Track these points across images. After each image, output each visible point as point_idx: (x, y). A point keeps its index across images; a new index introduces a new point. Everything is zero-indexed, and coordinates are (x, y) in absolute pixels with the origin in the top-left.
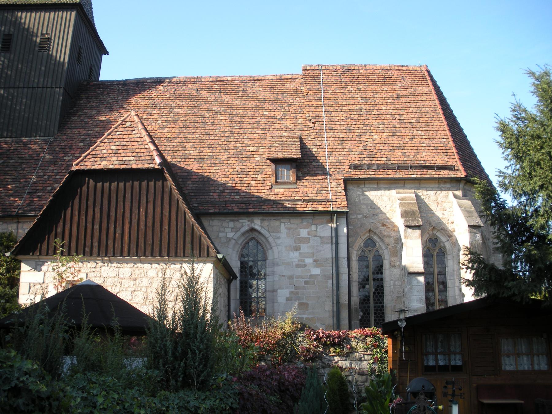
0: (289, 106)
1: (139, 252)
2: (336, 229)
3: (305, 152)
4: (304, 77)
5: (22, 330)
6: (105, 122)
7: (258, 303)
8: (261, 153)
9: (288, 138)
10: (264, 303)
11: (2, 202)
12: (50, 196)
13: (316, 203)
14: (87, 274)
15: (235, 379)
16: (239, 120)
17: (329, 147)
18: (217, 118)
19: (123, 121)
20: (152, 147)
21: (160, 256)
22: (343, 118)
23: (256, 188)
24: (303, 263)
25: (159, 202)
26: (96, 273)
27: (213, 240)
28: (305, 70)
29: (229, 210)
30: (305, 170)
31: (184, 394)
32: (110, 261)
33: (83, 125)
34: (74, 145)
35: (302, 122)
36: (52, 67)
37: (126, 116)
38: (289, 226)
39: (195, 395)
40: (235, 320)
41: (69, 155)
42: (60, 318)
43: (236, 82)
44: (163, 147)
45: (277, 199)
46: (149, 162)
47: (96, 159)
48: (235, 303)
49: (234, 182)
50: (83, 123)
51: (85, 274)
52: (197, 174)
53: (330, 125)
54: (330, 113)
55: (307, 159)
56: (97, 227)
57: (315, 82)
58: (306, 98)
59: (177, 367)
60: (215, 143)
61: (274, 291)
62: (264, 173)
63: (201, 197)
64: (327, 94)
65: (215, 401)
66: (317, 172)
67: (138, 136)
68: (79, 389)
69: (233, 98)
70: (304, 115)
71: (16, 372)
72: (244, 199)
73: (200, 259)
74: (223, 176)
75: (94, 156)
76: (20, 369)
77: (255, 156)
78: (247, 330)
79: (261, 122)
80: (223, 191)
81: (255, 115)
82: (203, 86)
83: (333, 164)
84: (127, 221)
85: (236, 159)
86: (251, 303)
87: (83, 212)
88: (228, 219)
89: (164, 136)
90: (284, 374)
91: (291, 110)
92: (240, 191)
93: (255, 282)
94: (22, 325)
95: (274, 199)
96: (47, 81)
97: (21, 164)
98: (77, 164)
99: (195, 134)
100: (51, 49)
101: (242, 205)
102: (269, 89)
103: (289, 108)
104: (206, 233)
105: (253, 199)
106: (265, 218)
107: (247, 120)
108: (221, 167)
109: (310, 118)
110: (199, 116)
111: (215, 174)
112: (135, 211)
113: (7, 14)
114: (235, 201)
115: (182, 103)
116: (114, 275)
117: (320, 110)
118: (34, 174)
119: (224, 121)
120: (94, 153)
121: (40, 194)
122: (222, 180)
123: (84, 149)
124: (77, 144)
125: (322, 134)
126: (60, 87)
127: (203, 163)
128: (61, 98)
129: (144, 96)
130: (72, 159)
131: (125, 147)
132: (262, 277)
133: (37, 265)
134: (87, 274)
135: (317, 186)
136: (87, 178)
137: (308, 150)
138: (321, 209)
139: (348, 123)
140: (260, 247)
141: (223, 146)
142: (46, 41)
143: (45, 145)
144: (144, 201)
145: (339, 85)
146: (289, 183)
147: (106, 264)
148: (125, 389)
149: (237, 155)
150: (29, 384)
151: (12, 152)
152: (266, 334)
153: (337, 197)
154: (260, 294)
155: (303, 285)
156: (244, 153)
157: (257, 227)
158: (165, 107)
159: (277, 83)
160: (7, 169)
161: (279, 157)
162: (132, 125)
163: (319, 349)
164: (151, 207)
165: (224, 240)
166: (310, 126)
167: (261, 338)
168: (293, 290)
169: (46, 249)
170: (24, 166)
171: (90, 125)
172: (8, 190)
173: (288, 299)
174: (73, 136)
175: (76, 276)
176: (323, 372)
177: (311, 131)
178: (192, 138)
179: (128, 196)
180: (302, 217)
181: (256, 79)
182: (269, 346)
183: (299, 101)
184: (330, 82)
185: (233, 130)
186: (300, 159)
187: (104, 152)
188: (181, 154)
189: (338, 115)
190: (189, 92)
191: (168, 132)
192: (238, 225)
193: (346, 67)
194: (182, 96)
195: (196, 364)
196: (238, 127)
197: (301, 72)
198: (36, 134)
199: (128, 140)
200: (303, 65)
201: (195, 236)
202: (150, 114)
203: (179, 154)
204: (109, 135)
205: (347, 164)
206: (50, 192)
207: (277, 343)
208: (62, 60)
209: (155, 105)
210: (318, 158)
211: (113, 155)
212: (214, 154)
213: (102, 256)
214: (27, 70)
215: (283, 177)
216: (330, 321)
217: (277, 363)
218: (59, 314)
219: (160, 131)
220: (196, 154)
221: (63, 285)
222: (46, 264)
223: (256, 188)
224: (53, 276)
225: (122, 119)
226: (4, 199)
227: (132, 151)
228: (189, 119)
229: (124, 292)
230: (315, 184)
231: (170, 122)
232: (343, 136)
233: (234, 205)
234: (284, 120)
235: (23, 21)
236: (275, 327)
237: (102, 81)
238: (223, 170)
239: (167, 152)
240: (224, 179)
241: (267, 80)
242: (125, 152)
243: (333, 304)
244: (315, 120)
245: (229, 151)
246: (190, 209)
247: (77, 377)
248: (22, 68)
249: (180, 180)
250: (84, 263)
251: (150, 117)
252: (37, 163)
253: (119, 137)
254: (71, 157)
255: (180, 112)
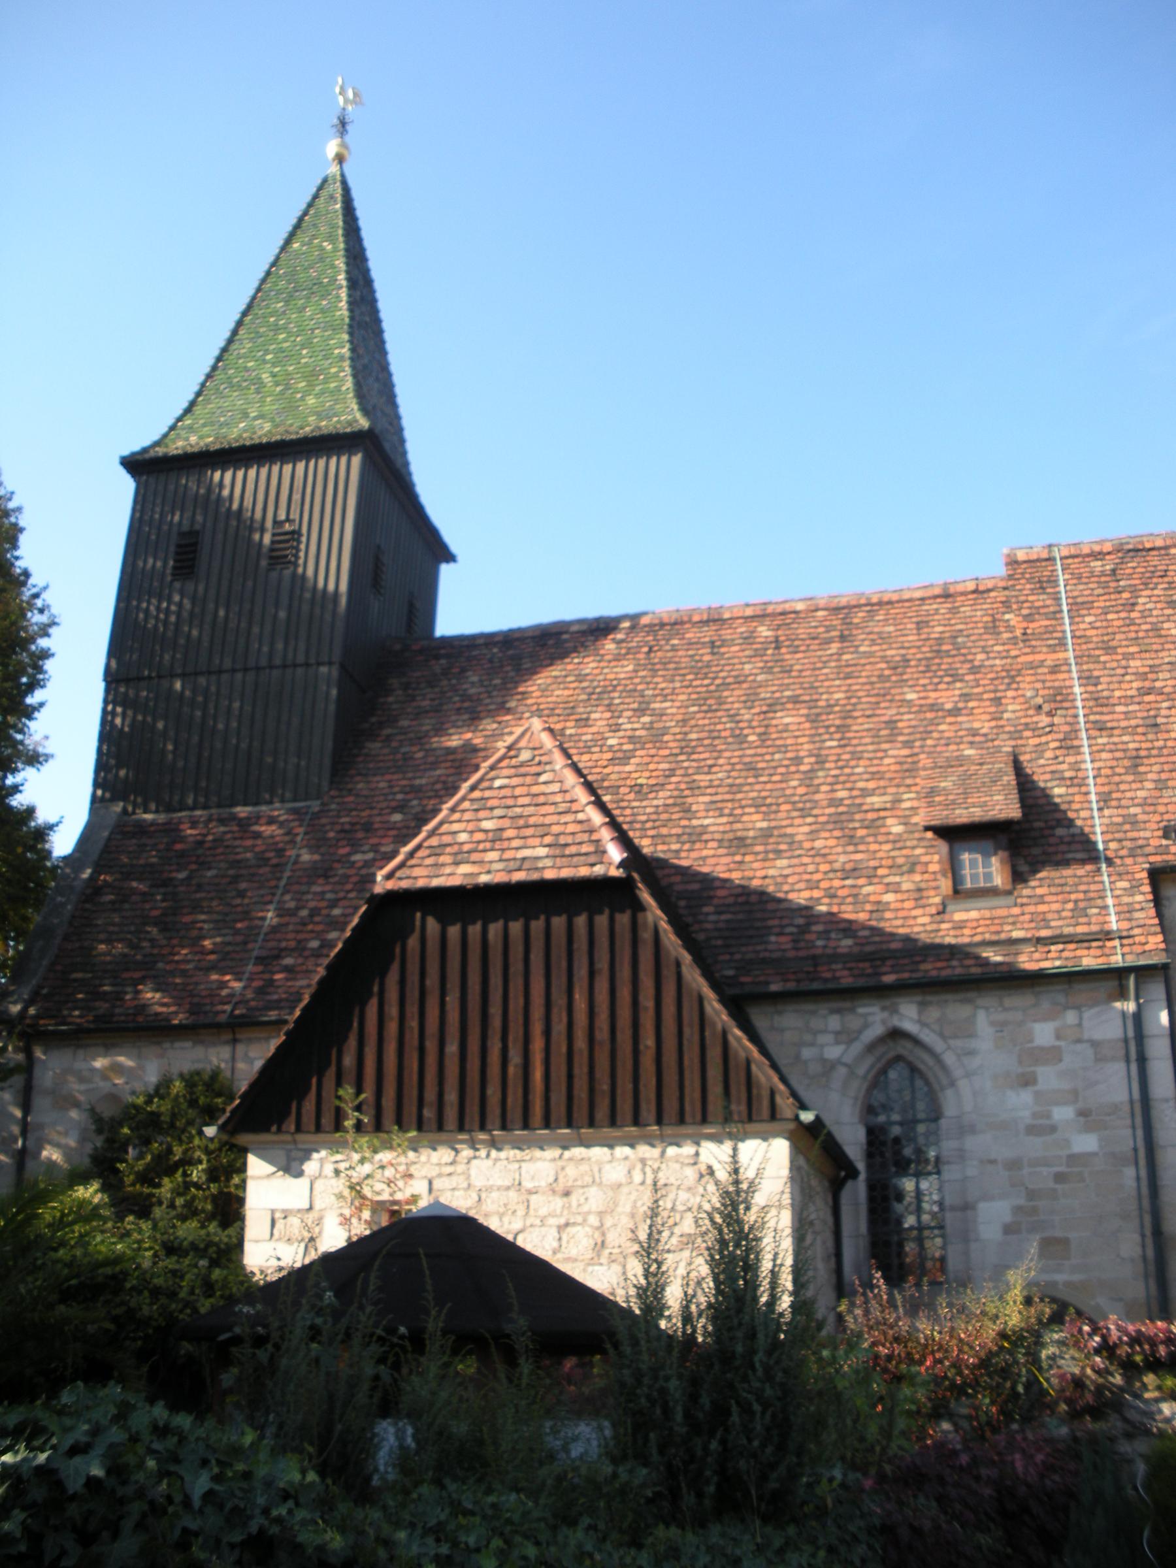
0: (975, 670)
1: (575, 1115)
2: (1138, 1017)
3: (1030, 802)
4: (1011, 583)
5: (263, 1355)
6: (460, 751)
7: (920, 1241)
8: (907, 813)
9: (981, 764)
10: (938, 1241)
11: (191, 987)
12: (317, 965)
13: (1072, 946)
14: (430, 1183)
15: (868, 1483)
16: (838, 722)
17: (1099, 780)
18: (774, 722)
19: (510, 748)
20: (597, 818)
21: (636, 1122)
22: (1133, 692)
23: (901, 914)
24: (1047, 1122)
25: (624, 973)
26: (454, 1178)
27: (785, 1070)
28: (1012, 562)
29: (826, 980)
30: (1036, 851)
31: (723, 1535)
32: (494, 1144)
33: (400, 763)
34: (378, 819)
35: (1018, 714)
36: (306, 608)
37: (518, 731)
38: (1001, 1017)
39: (754, 1536)
40: (859, 1300)
41: (366, 848)
42: (363, 1318)
43: (820, 613)
44: (628, 812)
45: (961, 940)
46: (592, 859)
47: (442, 859)
48: (854, 1248)
49: (835, 901)
50: (399, 756)
51: (425, 1184)
52: (728, 885)
53: (1098, 717)
54: (1093, 681)
55: (1039, 820)
56: (452, 1048)
57: (1045, 597)
58: (1021, 645)
59: (699, 1453)
60: (775, 794)
61: (967, 1207)
62: (919, 868)
63: (743, 949)
64: (1082, 626)
65: (814, 1555)
66: (1070, 856)
67: (555, 787)
68: (427, 1531)
69: (816, 660)
70: (1020, 692)
71: (259, 1492)
72: (868, 949)
73: (750, 1127)
74: (802, 885)
75: (436, 851)
76: (269, 1483)
77: (889, 821)
78: (896, 1328)
79: (900, 725)
80: (804, 929)
81: (882, 705)
82: (727, 634)
83: (1115, 828)
84: (537, 1029)
85: (837, 833)
86: (900, 1245)
87: (412, 1010)
88: (823, 1008)
89: (628, 782)
90: (1013, 1462)
91: (981, 682)
92: (854, 927)
93: (908, 1185)
94: (260, 1341)
95: (953, 941)
96: (295, 650)
97: (236, 879)
98: (389, 876)
99: (714, 769)
100: (301, 561)
101: (861, 965)
102: (913, 626)
103: (978, 676)
104: (764, 1051)
105: (894, 946)
106: (929, 998)
107: (860, 720)
108: (795, 861)
109: (1039, 700)
110: (724, 720)
111: (779, 880)
112: (559, 999)
113: (187, 481)
114: (843, 955)
115: (671, 685)
116: (507, 1183)
117: (1065, 676)
118: (271, 907)
119: (795, 727)
120: (434, 841)
121: (288, 961)
122: (800, 897)
123: (405, 831)
124: (386, 818)
125: (1076, 743)
126: (330, 663)
127: (743, 851)
128: (334, 692)
129: (564, 673)
130: (374, 860)
131: (521, 822)
132: (930, 1168)
133: (290, 1159)
134: (430, 1183)
135: (1073, 897)
136: (418, 915)
137: (1038, 793)
138: (1089, 960)
139: (1148, 707)
140: (919, 1083)
141: (797, 798)
142: (287, 541)
143: (296, 823)
144: (581, 972)
145: (1113, 597)
146: (993, 892)
147: (483, 1153)
148: (554, 1528)
149: (837, 821)
150: (297, 1528)
151: (210, 849)
152: (951, 1337)
153: (1134, 923)
154: (926, 1218)
155: (1051, 1184)
156: (857, 817)
157: (909, 1026)
158: (627, 700)
159: (935, 606)
160: (198, 895)
161: (960, 821)
162: (537, 759)
163: (1111, 1379)
164: (602, 986)
165: (814, 1068)
166: (1041, 725)
167: (938, 1350)
168: (1022, 1202)
169: (313, 1115)
170: (243, 886)
171: (418, 762)
172: (204, 952)
173: (1008, 1230)
174: (373, 796)
175: (400, 1190)
176: (1129, 1450)
177: (1044, 739)
178: (707, 784)
179: (537, 958)
180: (1037, 989)
181: (875, 600)
182: (960, 1373)
183: (1004, 654)
184: (1086, 593)
185: (824, 752)
186: (1018, 822)
187: (463, 837)
188: (679, 831)
189: (1116, 686)
190: (690, 653)
191: (639, 768)
192: (853, 1022)
193: (1128, 543)
194: (672, 666)
195: (756, 1443)
196: (834, 743)
197: (1001, 570)
198: (272, 796)
199: (526, 800)
200: (1005, 551)
201: (732, 1063)
202: (584, 722)
203: (674, 831)
204: (473, 788)
205: (1155, 826)
206: (317, 954)
207: (984, 1363)
208: (331, 587)
209: (599, 695)
210: (1071, 815)
211: (488, 845)
212: (773, 824)
213: (470, 1131)
214: (239, 621)
215: (974, 877)
216: (1138, 1290)
217: (989, 1423)
218: (361, 1308)
219: (617, 769)
220: (721, 828)
221: (366, 1215)
222: (315, 1156)
223: (901, 914)
224: (337, 1191)
225: (510, 740)
226: (194, 980)
227: (540, 831)
228: (695, 729)
229: (537, 1229)
230: (1068, 889)
231: (643, 740)
232: (1136, 745)
233: (839, 966)
234: (964, 712)
235: (226, 493)
236: (977, 1316)
237: (444, 639)
238: (800, 870)
239: (638, 826)
240: (806, 894)
241: (907, 601)
242: (522, 835)
243: (1143, 1236)
244: (1053, 705)
245: (815, 812)
246: (715, 985)
247: (420, 1495)
248: (227, 617)
249: (682, 903)
250: (421, 1150)
251: (585, 730)
252: (278, 875)
253: (503, 792)
254: (370, 856)
255: (669, 711)
